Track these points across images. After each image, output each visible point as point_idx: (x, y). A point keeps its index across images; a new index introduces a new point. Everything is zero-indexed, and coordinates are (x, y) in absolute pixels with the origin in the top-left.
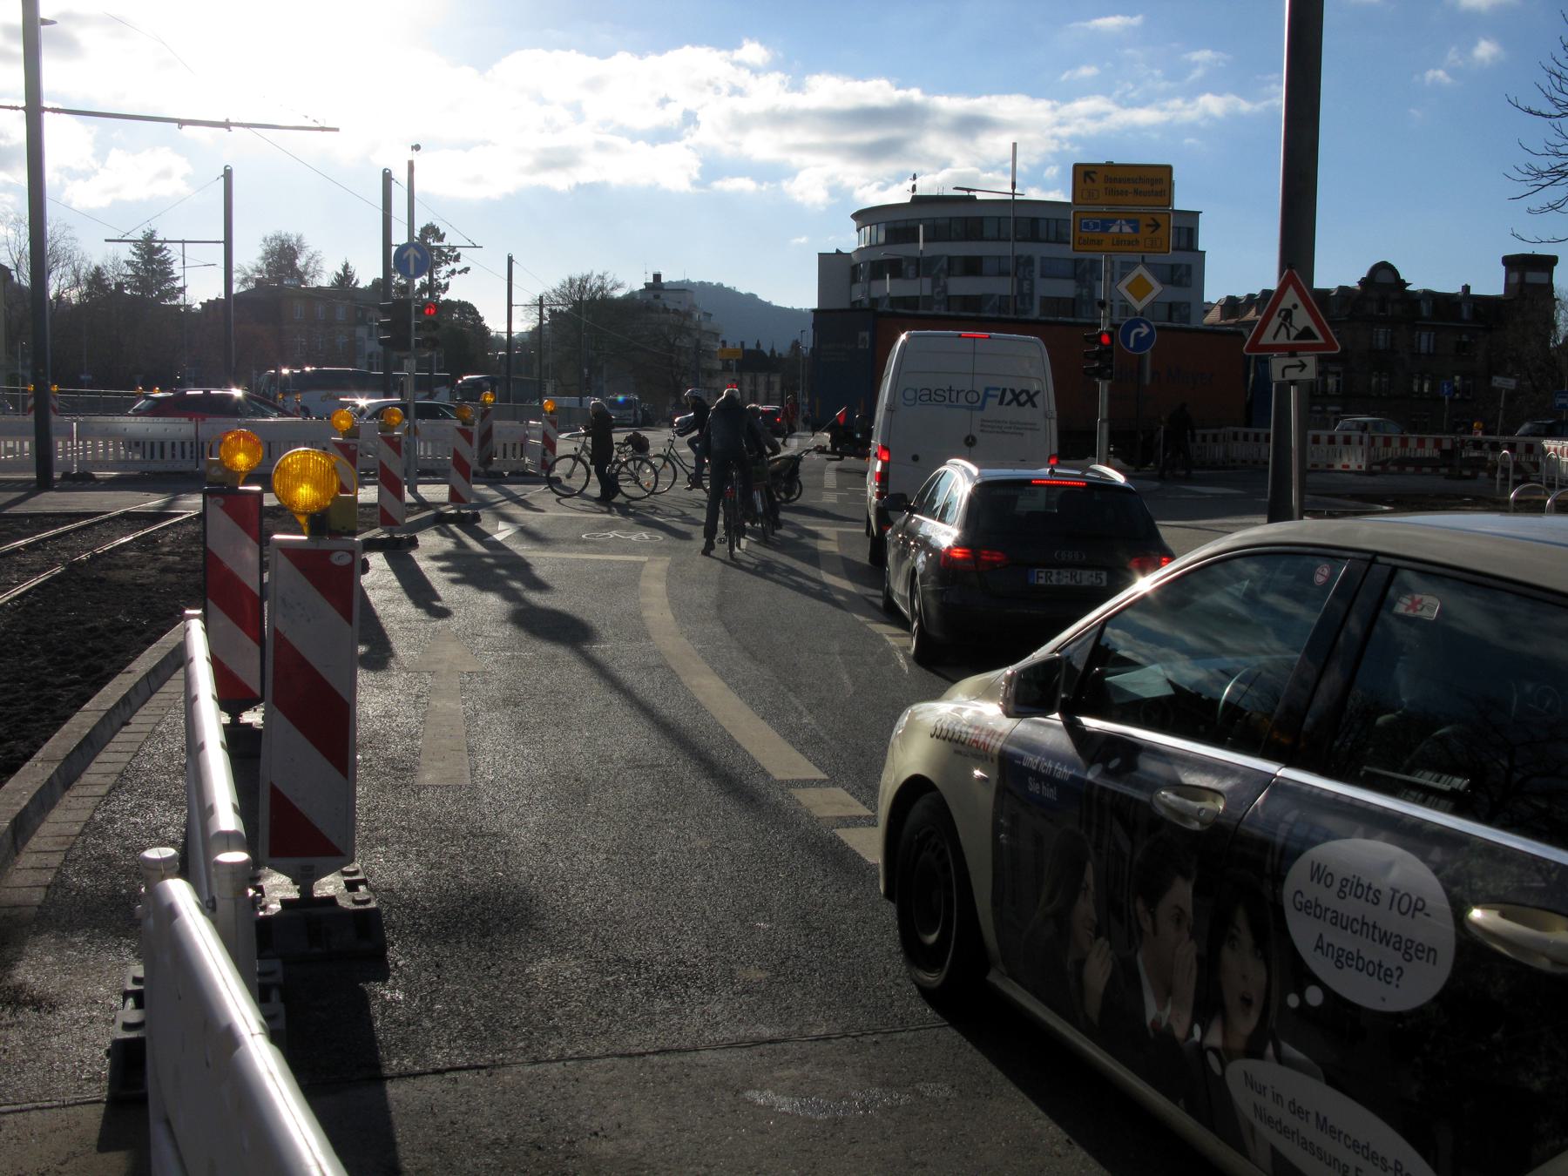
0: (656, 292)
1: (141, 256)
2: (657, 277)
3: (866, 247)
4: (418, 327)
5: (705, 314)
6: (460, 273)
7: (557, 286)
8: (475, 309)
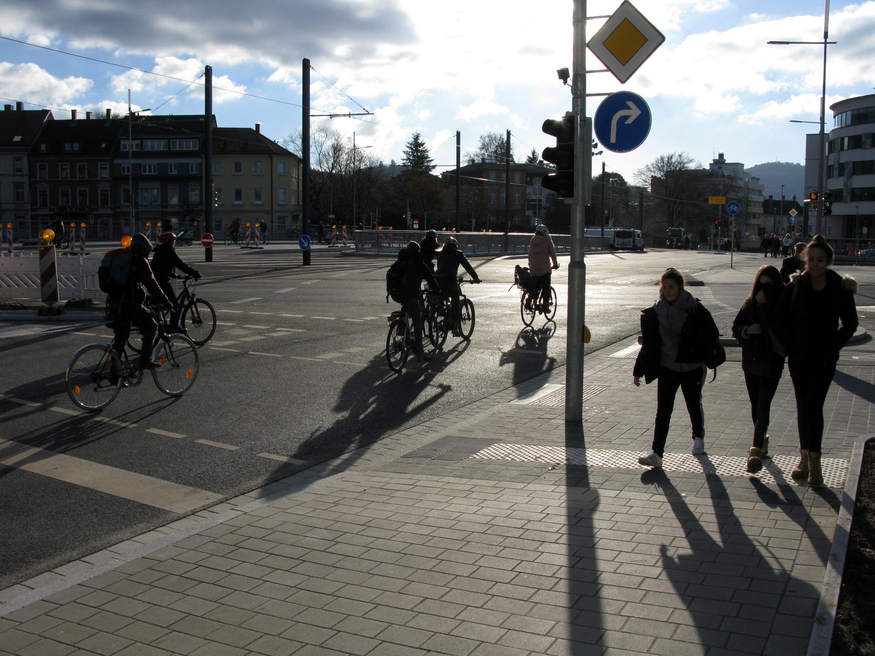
0: (720, 165)
1: (412, 149)
2: (721, 156)
3: (842, 128)
4: (67, 169)
5: (753, 178)
6: (596, 154)
7: (653, 161)
8: (622, 177)
